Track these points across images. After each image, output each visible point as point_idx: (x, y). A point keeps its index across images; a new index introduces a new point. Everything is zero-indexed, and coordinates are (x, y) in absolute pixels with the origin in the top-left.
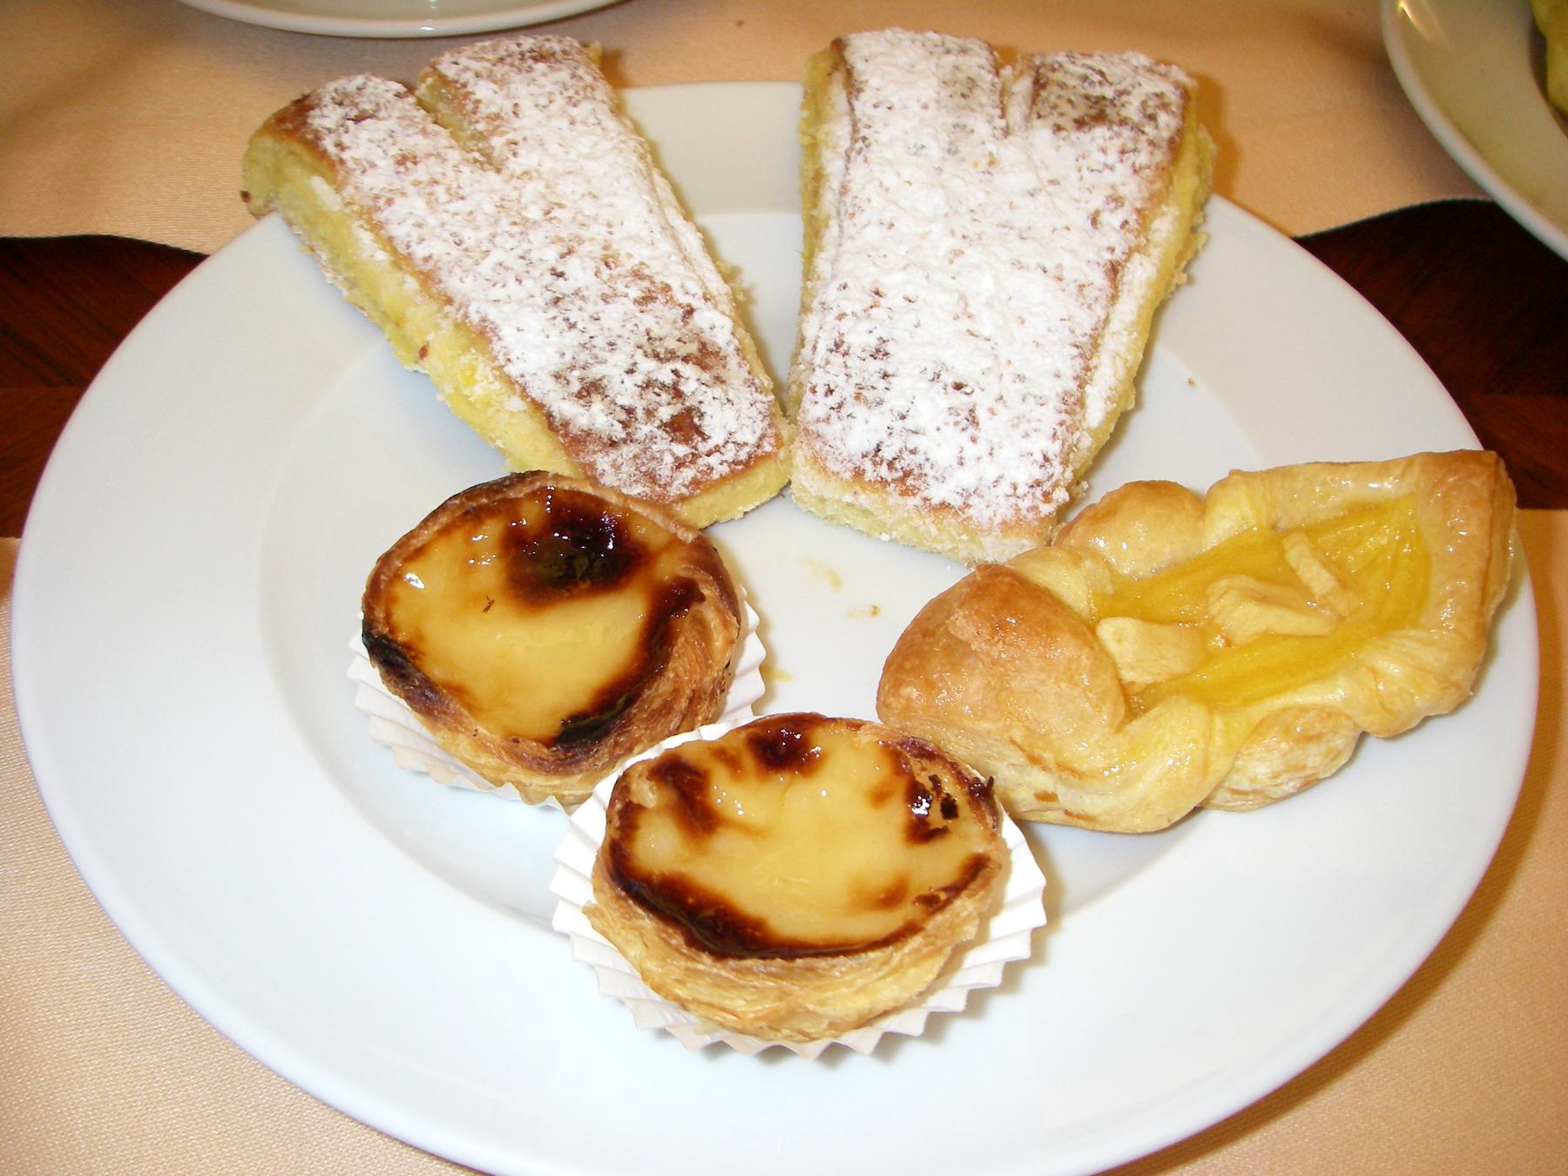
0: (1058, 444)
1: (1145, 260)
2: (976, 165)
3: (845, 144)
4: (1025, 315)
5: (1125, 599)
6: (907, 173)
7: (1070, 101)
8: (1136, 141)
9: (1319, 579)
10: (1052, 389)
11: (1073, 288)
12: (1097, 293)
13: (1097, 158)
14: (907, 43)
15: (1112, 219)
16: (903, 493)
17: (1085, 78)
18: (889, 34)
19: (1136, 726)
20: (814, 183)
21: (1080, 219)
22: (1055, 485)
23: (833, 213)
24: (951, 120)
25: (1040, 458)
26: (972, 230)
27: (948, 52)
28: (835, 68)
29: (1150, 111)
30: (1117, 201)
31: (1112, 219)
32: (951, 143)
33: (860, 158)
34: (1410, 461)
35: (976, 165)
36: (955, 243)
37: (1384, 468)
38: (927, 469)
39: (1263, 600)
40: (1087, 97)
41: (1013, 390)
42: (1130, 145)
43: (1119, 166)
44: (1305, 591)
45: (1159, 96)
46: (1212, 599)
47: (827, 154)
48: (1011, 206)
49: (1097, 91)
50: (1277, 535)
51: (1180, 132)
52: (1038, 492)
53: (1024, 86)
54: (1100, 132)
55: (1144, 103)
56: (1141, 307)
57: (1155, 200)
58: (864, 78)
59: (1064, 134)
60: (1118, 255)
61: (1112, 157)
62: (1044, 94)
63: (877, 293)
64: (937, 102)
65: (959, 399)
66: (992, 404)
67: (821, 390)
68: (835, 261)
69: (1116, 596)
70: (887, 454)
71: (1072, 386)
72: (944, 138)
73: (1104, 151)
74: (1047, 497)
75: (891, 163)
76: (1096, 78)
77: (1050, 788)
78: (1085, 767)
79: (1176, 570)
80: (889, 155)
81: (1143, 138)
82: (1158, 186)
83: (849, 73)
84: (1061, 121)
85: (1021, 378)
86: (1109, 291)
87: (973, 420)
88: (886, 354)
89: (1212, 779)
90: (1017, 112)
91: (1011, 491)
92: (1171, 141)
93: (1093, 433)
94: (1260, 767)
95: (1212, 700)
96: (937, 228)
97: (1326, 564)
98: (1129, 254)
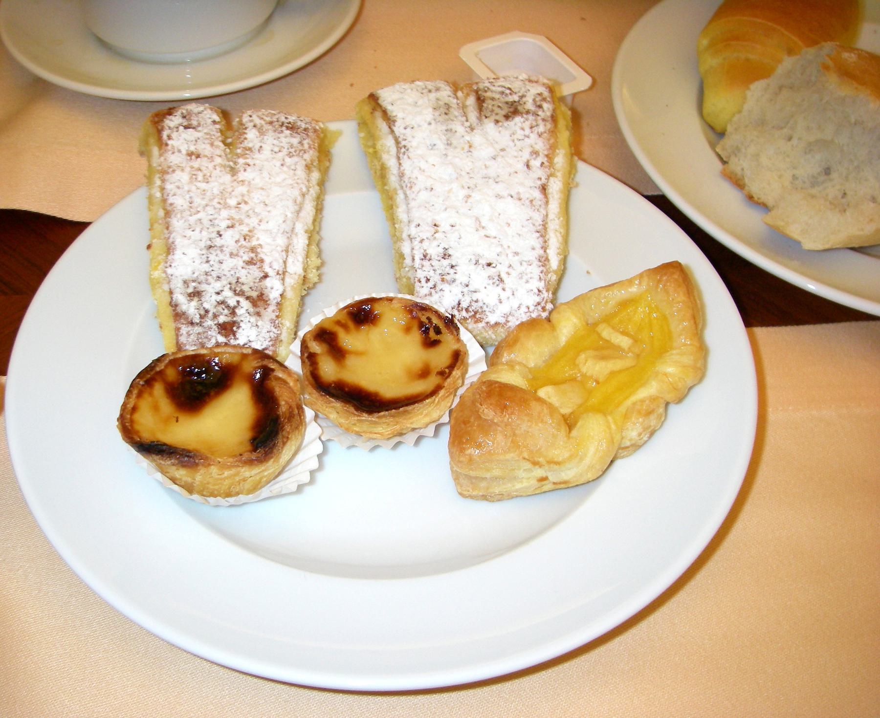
0: (543, 282)
1: (556, 179)
2: (463, 149)
3: (394, 150)
4: (509, 222)
5: (539, 378)
6: (432, 160)
7: (499, 107)
8: (536, 120)
9: (624, 342)
10: (532, 256)
11: (527, 202)
12: (540, 203)
13: (520, 134)
14: (409, 91)
15: (536, 163)
16: (476, 322)
17: (502, 93)
18: (397, 86)
19: (574, 433)
20: (381, 174)
21: (521, 166)
22: (546, 302)
23: (398, 187)
24: (444, 128)
25: (536, 291)
26: (471, 183)
27: (430, 91)
28: (374, 109)
29: (538, 103)
30: (535, 153)
31: (536, 163)
32: (448, 140)
33: (405, 157)
34: (641, 276)
35: (463, 149)
36: (465, 192)
37: (630, 282)
38: (485, 308)
39: (603, 358)
40: (507, 103)
41: (515, 260)
42: (534, 123)
43: (531, 135)
44: (618, 348)
45: (540, 94)
46: (581, 366)
47: (385, 157)
48: (486, 167)
49: (511, 99)
50: (591, 327)
51: (554, 110)
52: (539, 308)
53: (471, 101)
54: (518, 119)
55: (534, 100)
56: (560, 204)
57: (553, 148)
58: (394, 114)
59: (500, 124)
60: (544, 181)
61: (527, 131)
62: (485, 105)
63: (435, 225)
64: (435, 120)
65: (491, 271)
66: (507, 270)
67: (423, 280)
68: (408, 211)
69: (534, 378)
70: (464, 305)
71: (541, 252)
72: (444, 138)
73: (523, 129)
74: (544, 309)
75: (422, 157)
76: (508, 92)
77: (544, 475)
78: (561, 459)
79: (555, 358)
80: (419, 152)
81: (539, 118)
82: (552, 141)
83: (385, 113)
84: (497, 118)
85: (516, 254)
86: (544, 200)
87: (501, 280)
88: (450, 256)
89: (616, 445)
90: (473, 115)
91: (526, 310)
92: (552, 116)
93: (555, 272)
94: (633, 433)
95: (602, 409)
96: (455, 186)
97: (624, 333)
98: (549, 177)
